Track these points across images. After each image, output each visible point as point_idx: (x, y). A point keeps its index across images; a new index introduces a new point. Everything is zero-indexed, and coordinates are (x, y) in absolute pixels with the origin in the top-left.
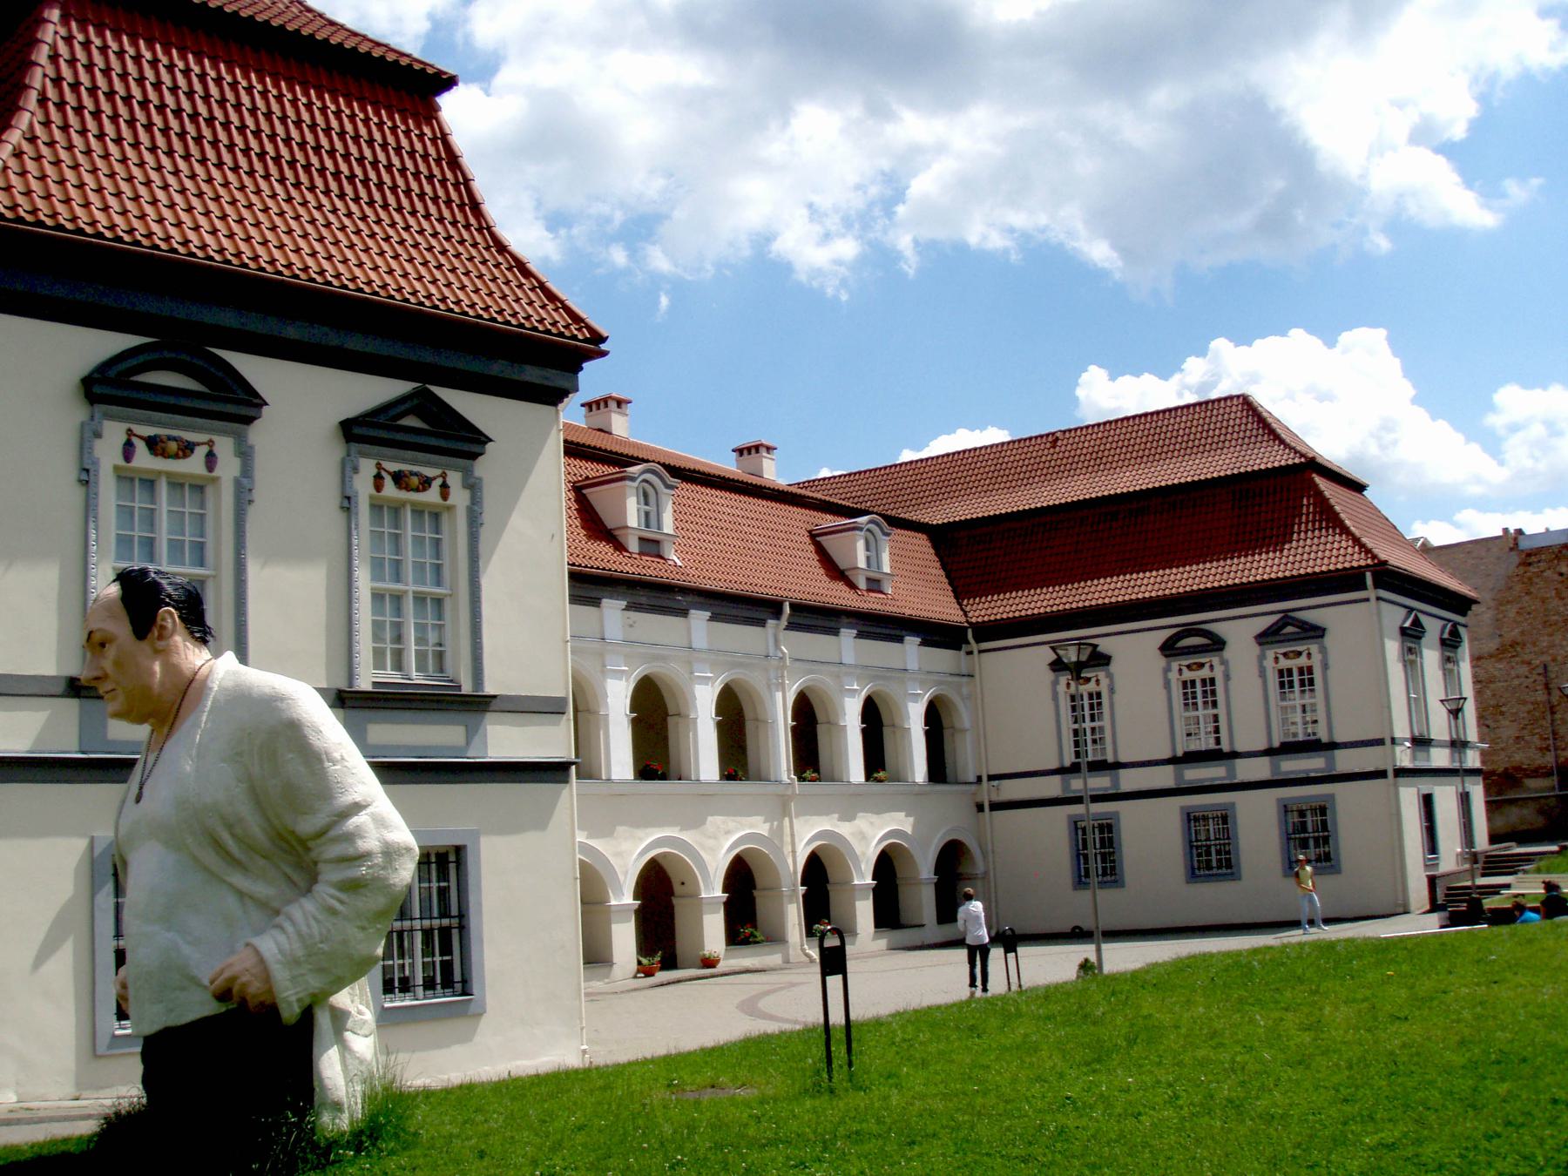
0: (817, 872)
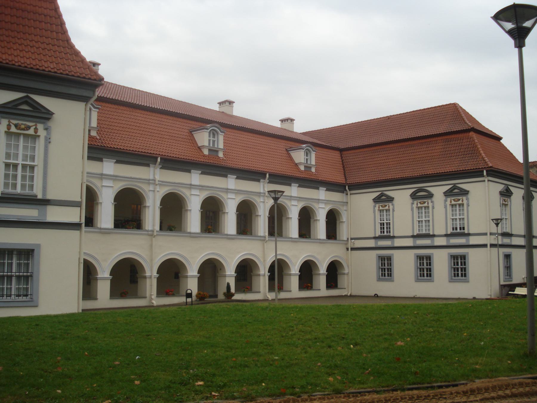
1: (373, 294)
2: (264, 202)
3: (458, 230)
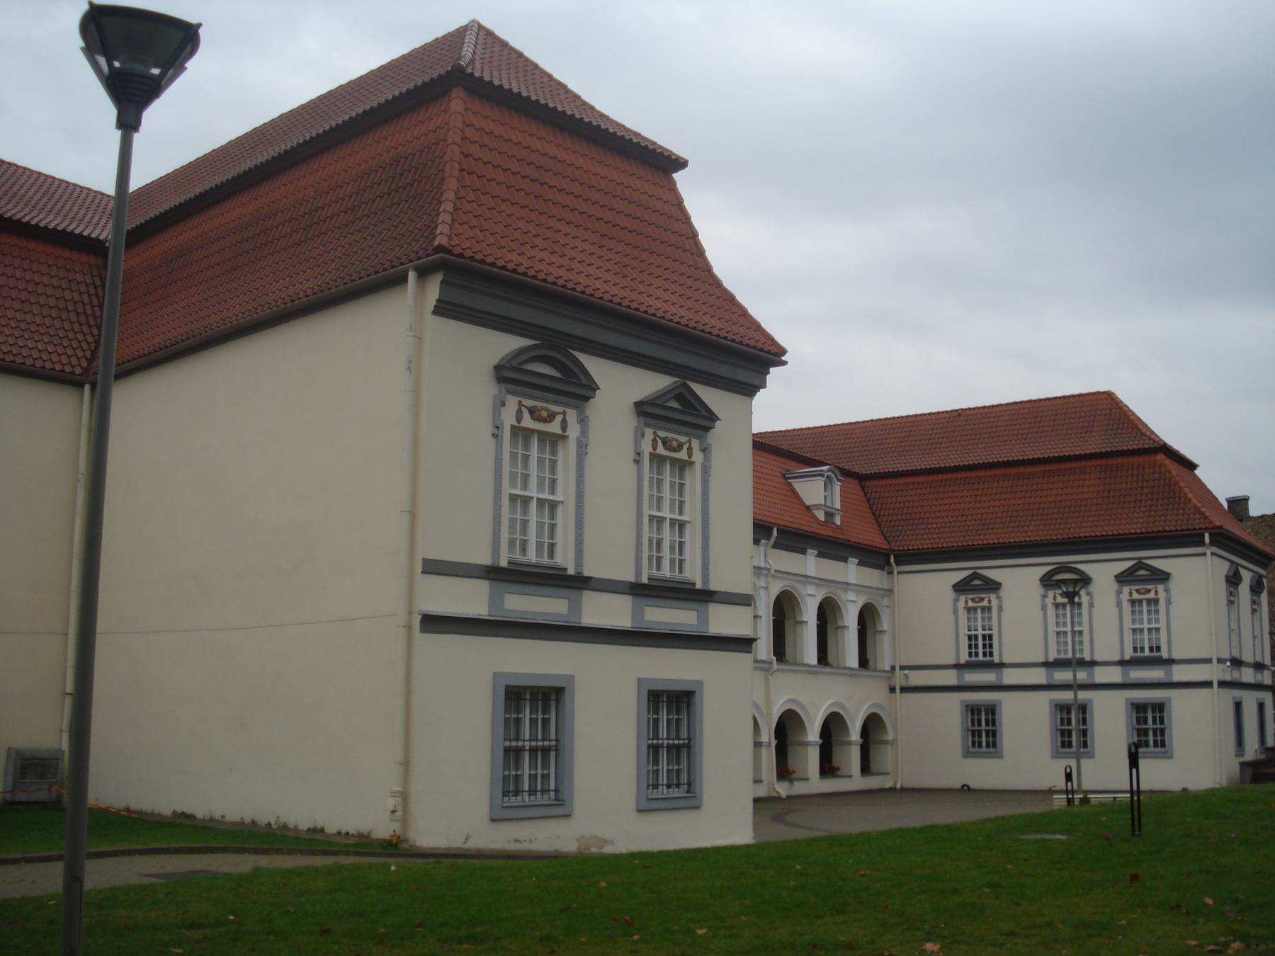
0: (833, 726)
1: (959, 786)
2: (766, 588)
3: (1147, 653)
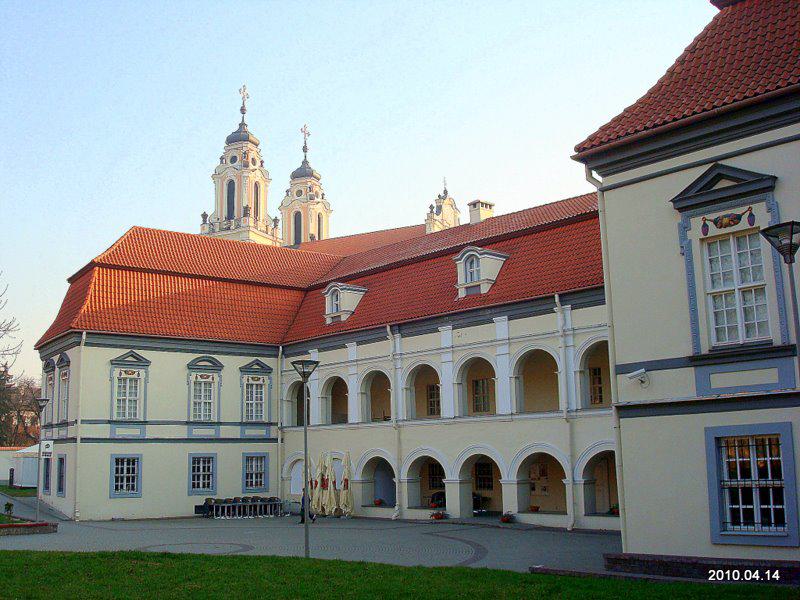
1: (110, 518)
